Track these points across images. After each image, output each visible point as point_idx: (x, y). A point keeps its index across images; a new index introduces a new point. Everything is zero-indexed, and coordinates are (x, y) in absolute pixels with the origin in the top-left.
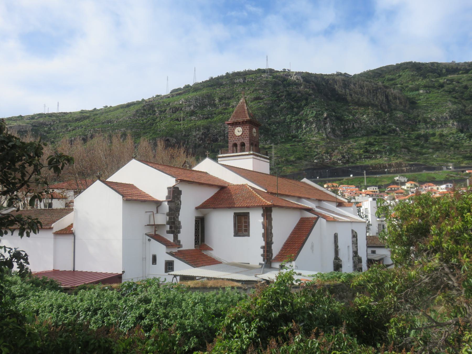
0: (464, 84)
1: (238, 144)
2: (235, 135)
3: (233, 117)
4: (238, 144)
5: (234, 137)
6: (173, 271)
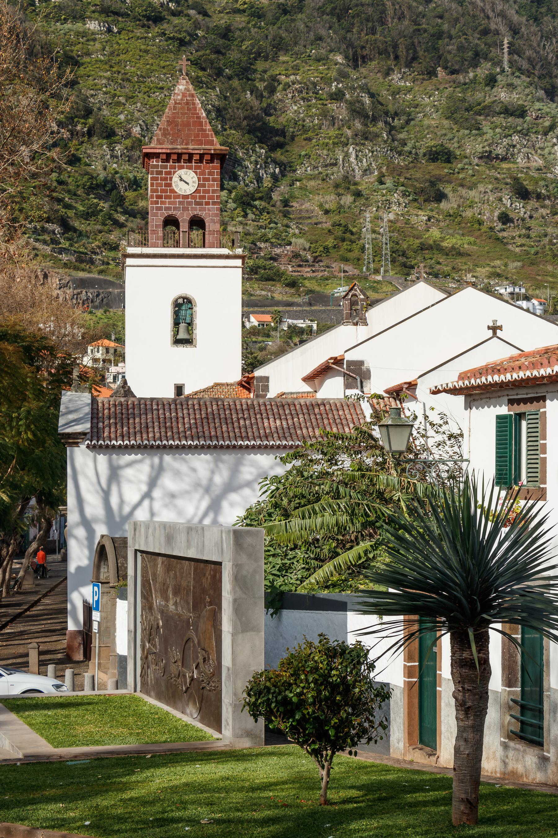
0: (222, 20)
1: (184, 219)
2: (173, 191)
3: (165, 133)
4: (184, 219)
5: (169, 197)
6: (499, 417)
